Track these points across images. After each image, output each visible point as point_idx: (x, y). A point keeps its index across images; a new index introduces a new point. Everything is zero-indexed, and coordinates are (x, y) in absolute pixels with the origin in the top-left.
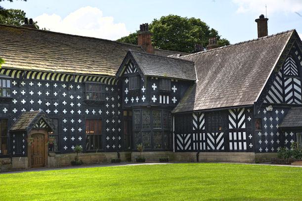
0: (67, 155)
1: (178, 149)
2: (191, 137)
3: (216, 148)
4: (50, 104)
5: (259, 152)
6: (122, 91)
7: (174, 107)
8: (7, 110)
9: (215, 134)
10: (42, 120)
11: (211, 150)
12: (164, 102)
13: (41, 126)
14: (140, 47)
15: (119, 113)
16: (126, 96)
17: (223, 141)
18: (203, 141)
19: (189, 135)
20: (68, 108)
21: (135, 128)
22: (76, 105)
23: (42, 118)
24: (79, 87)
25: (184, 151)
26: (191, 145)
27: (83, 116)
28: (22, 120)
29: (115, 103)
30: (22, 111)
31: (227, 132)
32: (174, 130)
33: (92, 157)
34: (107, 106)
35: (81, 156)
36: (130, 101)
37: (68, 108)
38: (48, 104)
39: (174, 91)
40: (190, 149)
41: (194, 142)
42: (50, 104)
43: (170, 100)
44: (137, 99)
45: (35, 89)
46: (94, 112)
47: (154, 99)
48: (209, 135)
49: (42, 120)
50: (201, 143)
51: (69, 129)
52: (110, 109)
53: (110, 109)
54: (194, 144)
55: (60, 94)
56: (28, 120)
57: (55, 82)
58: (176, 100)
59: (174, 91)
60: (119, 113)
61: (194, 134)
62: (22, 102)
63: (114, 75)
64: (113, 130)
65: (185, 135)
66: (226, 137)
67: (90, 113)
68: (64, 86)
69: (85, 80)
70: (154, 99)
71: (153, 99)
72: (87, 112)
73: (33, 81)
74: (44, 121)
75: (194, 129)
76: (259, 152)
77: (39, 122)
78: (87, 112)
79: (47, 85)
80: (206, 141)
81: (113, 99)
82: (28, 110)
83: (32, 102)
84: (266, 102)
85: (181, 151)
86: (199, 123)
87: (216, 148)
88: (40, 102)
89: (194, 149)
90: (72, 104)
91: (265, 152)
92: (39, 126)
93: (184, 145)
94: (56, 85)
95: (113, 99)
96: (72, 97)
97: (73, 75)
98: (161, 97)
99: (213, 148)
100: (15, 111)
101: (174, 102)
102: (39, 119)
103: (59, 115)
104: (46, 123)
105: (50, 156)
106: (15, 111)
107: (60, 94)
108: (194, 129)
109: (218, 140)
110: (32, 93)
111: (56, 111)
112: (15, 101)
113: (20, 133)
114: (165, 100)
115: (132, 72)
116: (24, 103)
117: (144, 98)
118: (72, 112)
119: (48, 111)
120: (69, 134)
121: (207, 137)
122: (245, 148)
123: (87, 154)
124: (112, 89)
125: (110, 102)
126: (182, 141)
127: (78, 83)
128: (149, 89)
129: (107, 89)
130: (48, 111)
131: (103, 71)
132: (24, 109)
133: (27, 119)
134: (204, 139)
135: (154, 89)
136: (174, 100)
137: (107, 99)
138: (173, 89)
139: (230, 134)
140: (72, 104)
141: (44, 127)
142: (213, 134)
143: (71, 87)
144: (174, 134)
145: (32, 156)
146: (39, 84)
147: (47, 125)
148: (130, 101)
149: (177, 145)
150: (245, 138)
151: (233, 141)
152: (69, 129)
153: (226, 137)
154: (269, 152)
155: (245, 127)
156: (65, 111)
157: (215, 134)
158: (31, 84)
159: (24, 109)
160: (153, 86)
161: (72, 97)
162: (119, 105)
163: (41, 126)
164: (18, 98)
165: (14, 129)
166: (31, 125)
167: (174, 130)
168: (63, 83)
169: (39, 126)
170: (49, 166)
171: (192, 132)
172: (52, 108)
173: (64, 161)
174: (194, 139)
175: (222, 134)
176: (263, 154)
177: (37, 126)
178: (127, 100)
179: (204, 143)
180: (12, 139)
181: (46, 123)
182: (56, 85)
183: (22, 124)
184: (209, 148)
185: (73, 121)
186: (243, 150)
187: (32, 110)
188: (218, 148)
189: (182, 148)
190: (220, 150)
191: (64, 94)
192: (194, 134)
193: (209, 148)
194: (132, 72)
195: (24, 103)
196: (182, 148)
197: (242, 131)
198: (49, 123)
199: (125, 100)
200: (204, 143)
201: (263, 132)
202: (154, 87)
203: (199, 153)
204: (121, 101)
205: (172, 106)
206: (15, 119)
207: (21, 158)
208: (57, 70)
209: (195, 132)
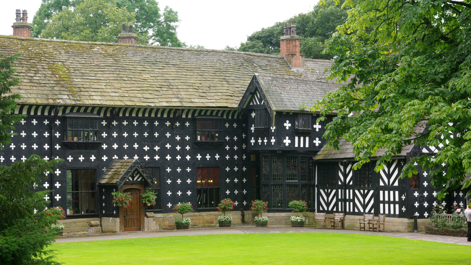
0: (171, 215)
1: (321, 209)
2: (336, 194)
3: (328, 209)
4: (148, 148)
6: (247, 131)
7: (318, 152)
8: (95, 158)
9: (364, 192)
10: (136, 172)
11: (359, 213)
13: (135, 179)
14: (283, 58)
15: (244, 157)
16: (252, 135)
17: (372, 202)
18: (350, 201)
19: (334, 191)
20: (173, 152)
21: (263, 181)
22: (183, 149)
23: (136, 170)
24: (187, 124)
25: (328, 212)
26: (336, 205)
28: (113, 170)
29: (239, 143)
30: (113, 158)
31: (377, 189)
32: (316, 183)
34: (227, 148)
35: (187, 219)
36: (256, 142)
37: (173, 152)
38: (146, 148)
39: (317, 130)
40: (335, 210)
42: (148, 148)
44: (266, 141)
45: (130, 129)
46: (208, 157)
47: (287, 141)
48: (357, 192)
49: (136, 172)
50: (347, 203)
51: (174, 181)
52: (232, 153)
53: (232, 153)
54: (340, 203)
55: (162, 135)
56: (120, 171)
57: (156, 118)
58: (320, 142)
59: (317, 130)
60: (244, 157)
61: (340, 190)
62: (113, 146)
63: (236, 106)
64: (236, 180)
65: (329, 190)
67: (204, 158)
68: (168, 124)
69: (196, 115)
70: (287, 141)
71: (285, 141)
72: (199, 157)
73: (127, 119)
74: (139, 172)
75: (340, 183)
77: (133, 174)
78: (199, 157)
79: (146, 123)
80: (353, 200)
81: (235, 138)
82: (121, 157)
83: (126, 146)
84: (427, 152)
85: (324, 211)
86: (345, 176)
87: (328, 209)
88: (136, 146)
89: (340, 210)
90: (178, 148)
91: (424, 217)
92: (133, 179)
93: (328, 204)
94: (156, 123)
95: (235, 138)
96: (178, 138)
97: (179, 110)
98: (297, 138)
99: (362, 210)
100: (105, 158)
101: (317, 145)
102: (133, 171)
103: (161, 162)
104: (141, 175)
105: (147, 217)
106: (105, 158)
107: (162, 135)
108: (340, 183)
109: (367, 200)
110: (126, 135)
111: (157, 158)
112: (105, 146)
113: (110, 187)
114: (302, 143)
115: (259, 104)
117: (273, 141)
118: (179, 158)
119: (147, 158)
120: (174, 187)
121: (354, 194)
122: (397, 213)
124: (235, 125)
125: (231, 143)
126: (362, 200)
127: (187, 119)
128: (280, 127)
129: (227, 125)
130: (147, 158)
131: (221, 101)
132: (115, 156)
133: (119, 170)
134: (351, 198)
135: (287, 128)
136: (317, 142)
137: (227, 138)
138: (315, 126)
139: (381, 192)
140: (178, 148)
141: (139, 180)
142: (362, 191)
143: (178, 124)
144: (316, 189)
145: (124, 217)
146: (135, 123)
147: (143, 178)
148: (256, 142)
149: (319, 204)
150: (397, 199)
151: (384, 202)
152: (174, 181)
153: (376, 196)
154: (428, 217)
155: (397, 185)
156: (168, 158)
157: (364, 192)
158: (125, 123)
159: (115, 156)
160: (285, 125)
161: (178, 138)
162: (244, 146)
163: (135, 179)
164: (108, 142)
165: (104, 181)
166: (123, 178)
167: (316, 183)
169: (133, 179)
170: (146, 230)
171: (338, 187)
172: (152, 153)
173: (167, 223)
174: (340, 197)
175: (372, 192)
177: (131, 179)
178: (253, 141)
179: (351, 203)
180: (101, 194)
181: (141, 175)
182: (156, 123)
183: (112, 178)
184: (356, 211)
185: (179, 170)
186: (394, 215)
187: (126, 157)
188: (367, 210)
189: (326, 209)
191: (168, 135)
192: (340, 190)
193: (356, 211)
194: (259, 104)
196: (326, 209)
197: (394, 189)
198: (145, 175)
199: (251, 141)
200: (351, 203)
201: (421, 192)
202: (287, 125)
204: (247, 141)
205: (314, 150)
206: (104, 169)
207: (111, 218)
208: (158, 105)
209: (341, 187)
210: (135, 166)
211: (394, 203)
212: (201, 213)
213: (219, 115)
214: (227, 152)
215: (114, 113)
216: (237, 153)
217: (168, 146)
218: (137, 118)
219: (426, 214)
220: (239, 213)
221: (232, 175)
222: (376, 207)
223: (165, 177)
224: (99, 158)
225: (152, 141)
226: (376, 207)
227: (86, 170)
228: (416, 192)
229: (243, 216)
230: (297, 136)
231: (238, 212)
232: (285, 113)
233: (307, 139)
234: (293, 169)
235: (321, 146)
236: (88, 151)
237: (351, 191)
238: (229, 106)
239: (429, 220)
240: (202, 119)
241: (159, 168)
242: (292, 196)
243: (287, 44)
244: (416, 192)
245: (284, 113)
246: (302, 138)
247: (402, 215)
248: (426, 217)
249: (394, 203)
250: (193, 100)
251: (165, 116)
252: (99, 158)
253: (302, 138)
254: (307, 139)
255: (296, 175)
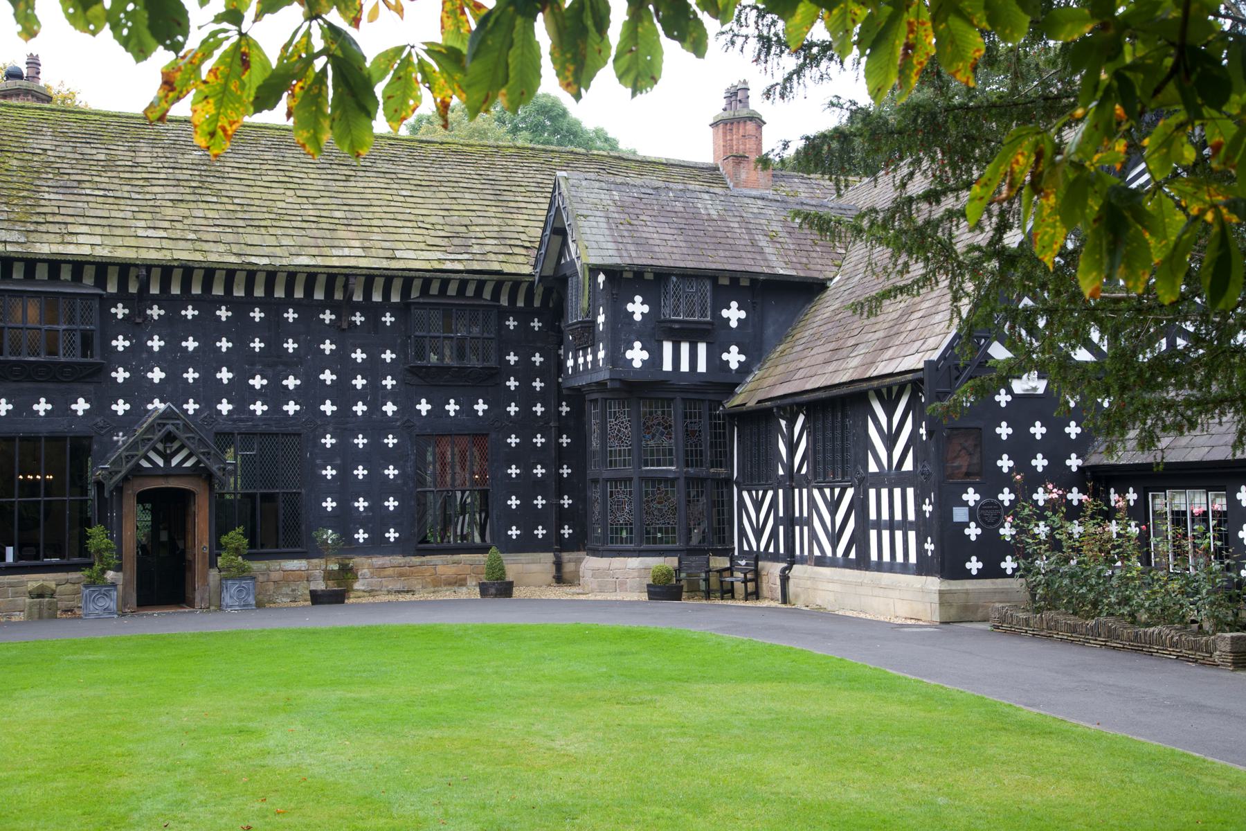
3: (834, 552)
5: (967, 575)
7: (737, 385)
12: (685, 367)
15: (565, 409)
24: (388, 319)
27: (406, 422)
30: (150, 407)
33: (440, 569)
34: (512, 383)
41: (878, 525)
43: (712, 357)
57: (386, 305)
58: (743, 358)
60: (565, 409)
65: (761, 493)
66: (860, 505)
67: (438, 411)
69: (415, 294)
72: (424, 407)
73: (196, 302)
76: (967, 575)
78: (424, 407)
80: (808, 521)
87: (834, 552)
91: (1002, 574)
98: (668, 347)
101: (734, 366)
114: (685, 359)
116: (156, 381)
119: (259, 408)
121: (812, 504)
122: (913, 559)
123: (424, 559)
136: (734, 357)
137: (512, 358)
141: (188, 464)
144: (735, 489)
150: (911, 516)
151: (878, 525)
154: (982, 574)
168: (322, 307)
171: (776, 484)
175: (850, 492)
176: (987, 584)
179: (806, 528)
184: (817, 552)
189: (829, 553)
190: (847, 563)
193: (817, 552)
195: (156, 381)
196: (829, 553)
200: (806, 528)
202: (638, 308)
203: (790, 568)
210: (165, 425)
211: (905, 525)
212: (428, 558)
213: (487, 295)
214: (511, 396)
215: (138, 283)
216: (542, 397)
217: (328, 377)
218: (228, 300)
219: (1008, 564)
220: (549, 557)
221: (525, 456)
222: (860, 539)
223: (318, 462)
224: (101, 406)
225: (275, 363)
226: (860, 539)
227: (55, 439)
228: (971, 490)
229: (559, 565)
230: (668, 340)
231: (542, 555)
232: (630, 275)
233: (702, 348)
234: (662, 434)
235: (745, 369)
236: (63, 386)
237: (805, 491)
238: (506, 270)
239: (1017, 584)
240: (424, 302)
241: (299, 435)
242: (660, 510)
243: (725, 134)
244: (971, 490)
245: (626, 275)
246: (685, 348)
247: (924, 567)
248: (1009, 572)
249: (905, 525)
250: (398, 254)
251: (319, 295)
252: (101, 406)
253: (685, 348)
254: (702, 348)
255: (671, 451)
